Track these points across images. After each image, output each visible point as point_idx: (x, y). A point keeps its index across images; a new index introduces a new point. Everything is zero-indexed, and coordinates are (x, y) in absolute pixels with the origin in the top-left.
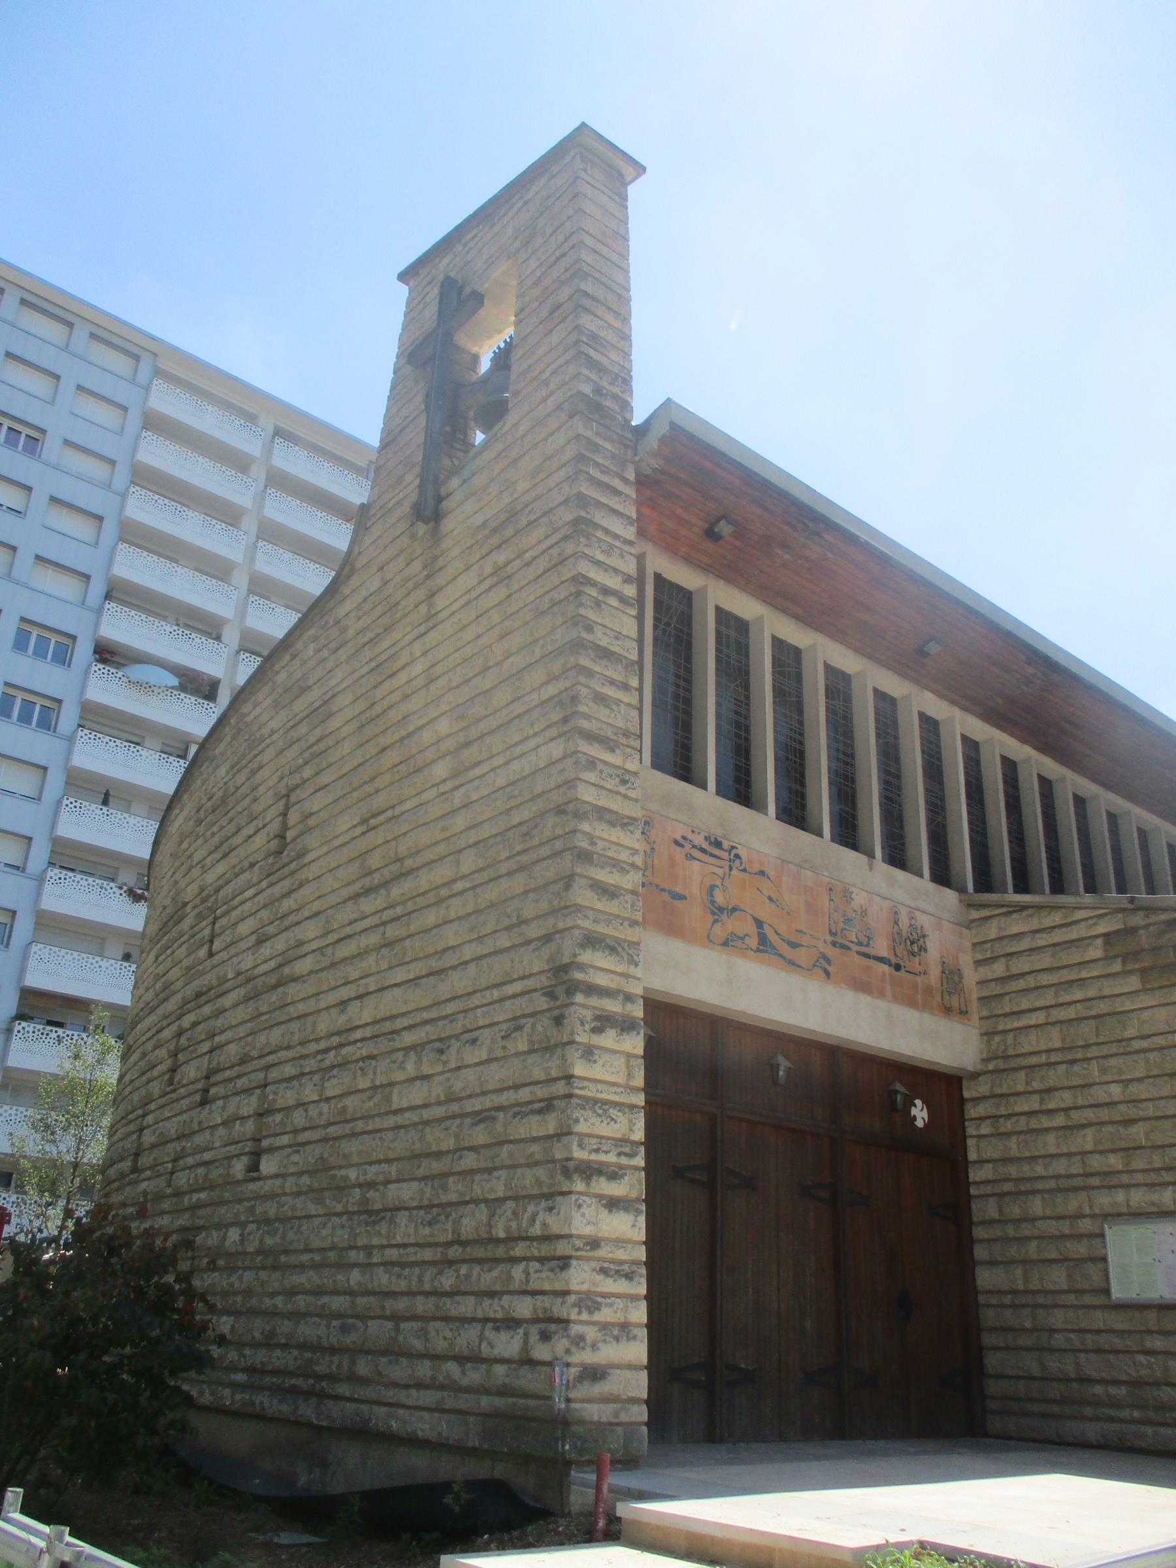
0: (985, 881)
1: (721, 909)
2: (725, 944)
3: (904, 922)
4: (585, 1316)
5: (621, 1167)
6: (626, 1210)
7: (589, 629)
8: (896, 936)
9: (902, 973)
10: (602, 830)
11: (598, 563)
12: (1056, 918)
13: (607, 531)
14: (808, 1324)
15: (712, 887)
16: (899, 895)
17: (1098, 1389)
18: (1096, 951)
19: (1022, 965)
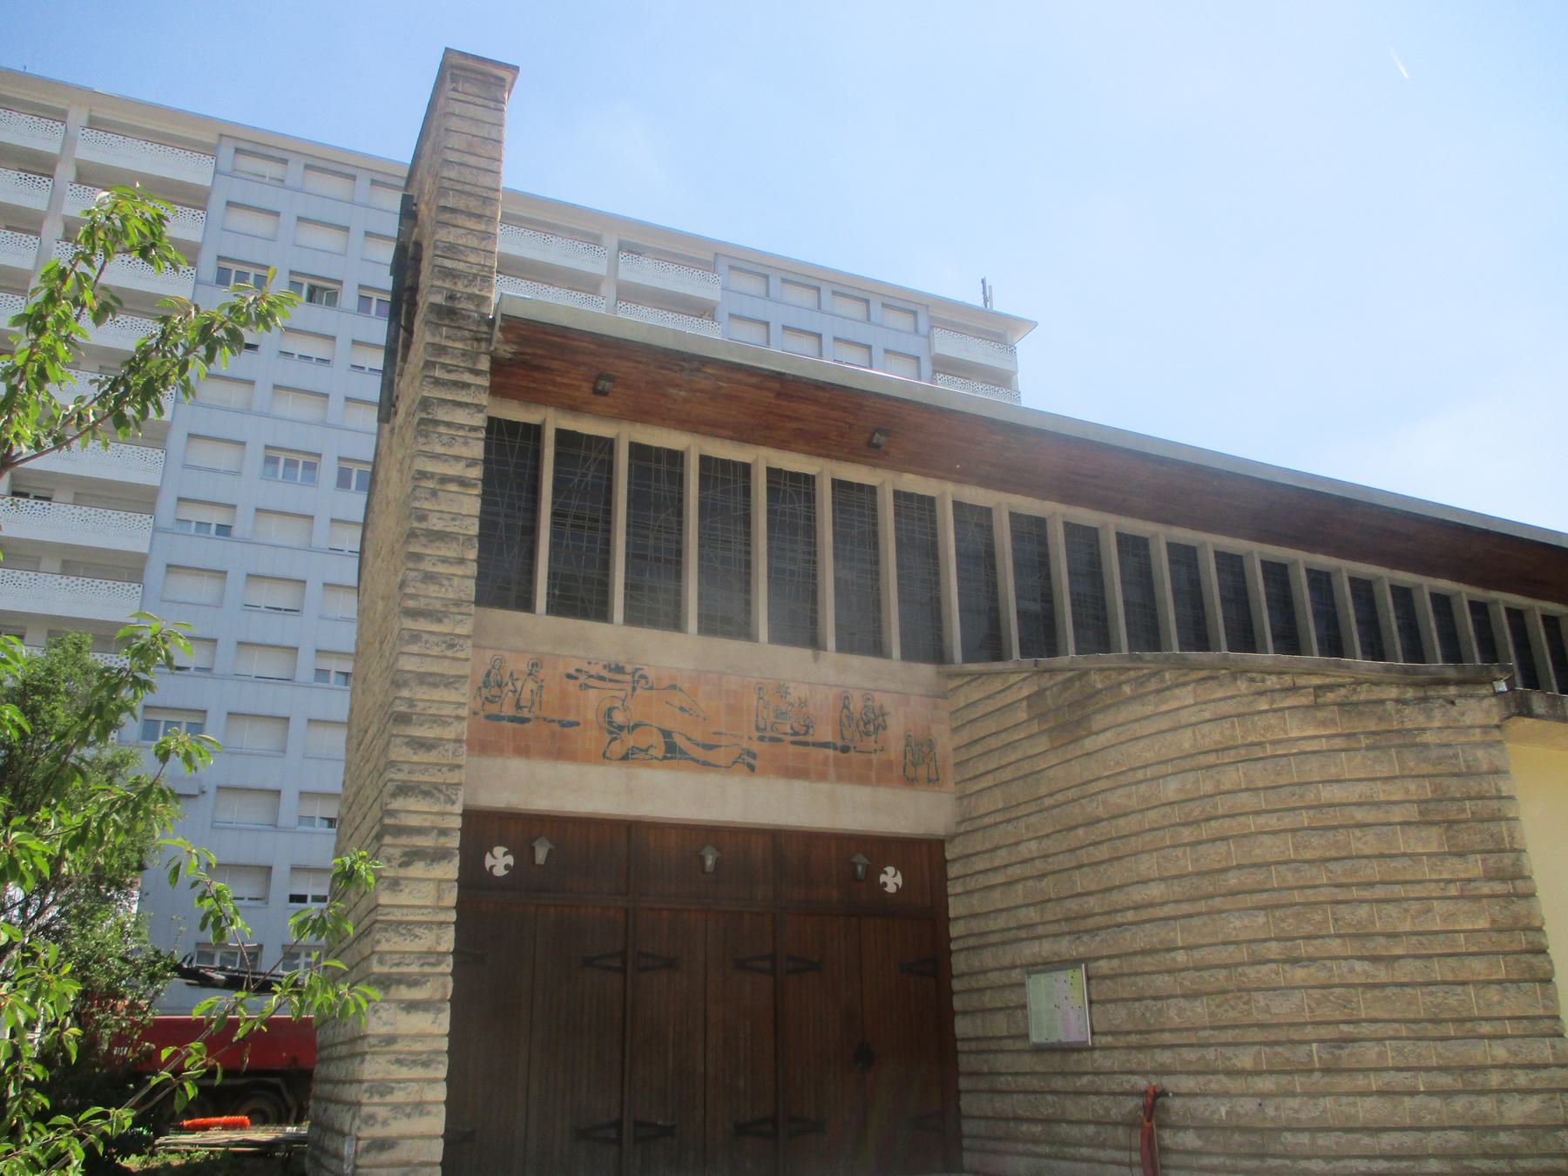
1: (621, 728)
2: (625, 758)
3: (857, 705)
4: (376, 1099)
5: (425, 975)
6: (426, 1010)
7: (422, 518)
8: (844, 720)
9: (852, 753)
10: (421, 693)
11: (435, 457)
12: (997, 684)
13: (449, 425)
14: (741, 1083)
15: (610, 710)
18: (1022, 715)
19: (980, 730)
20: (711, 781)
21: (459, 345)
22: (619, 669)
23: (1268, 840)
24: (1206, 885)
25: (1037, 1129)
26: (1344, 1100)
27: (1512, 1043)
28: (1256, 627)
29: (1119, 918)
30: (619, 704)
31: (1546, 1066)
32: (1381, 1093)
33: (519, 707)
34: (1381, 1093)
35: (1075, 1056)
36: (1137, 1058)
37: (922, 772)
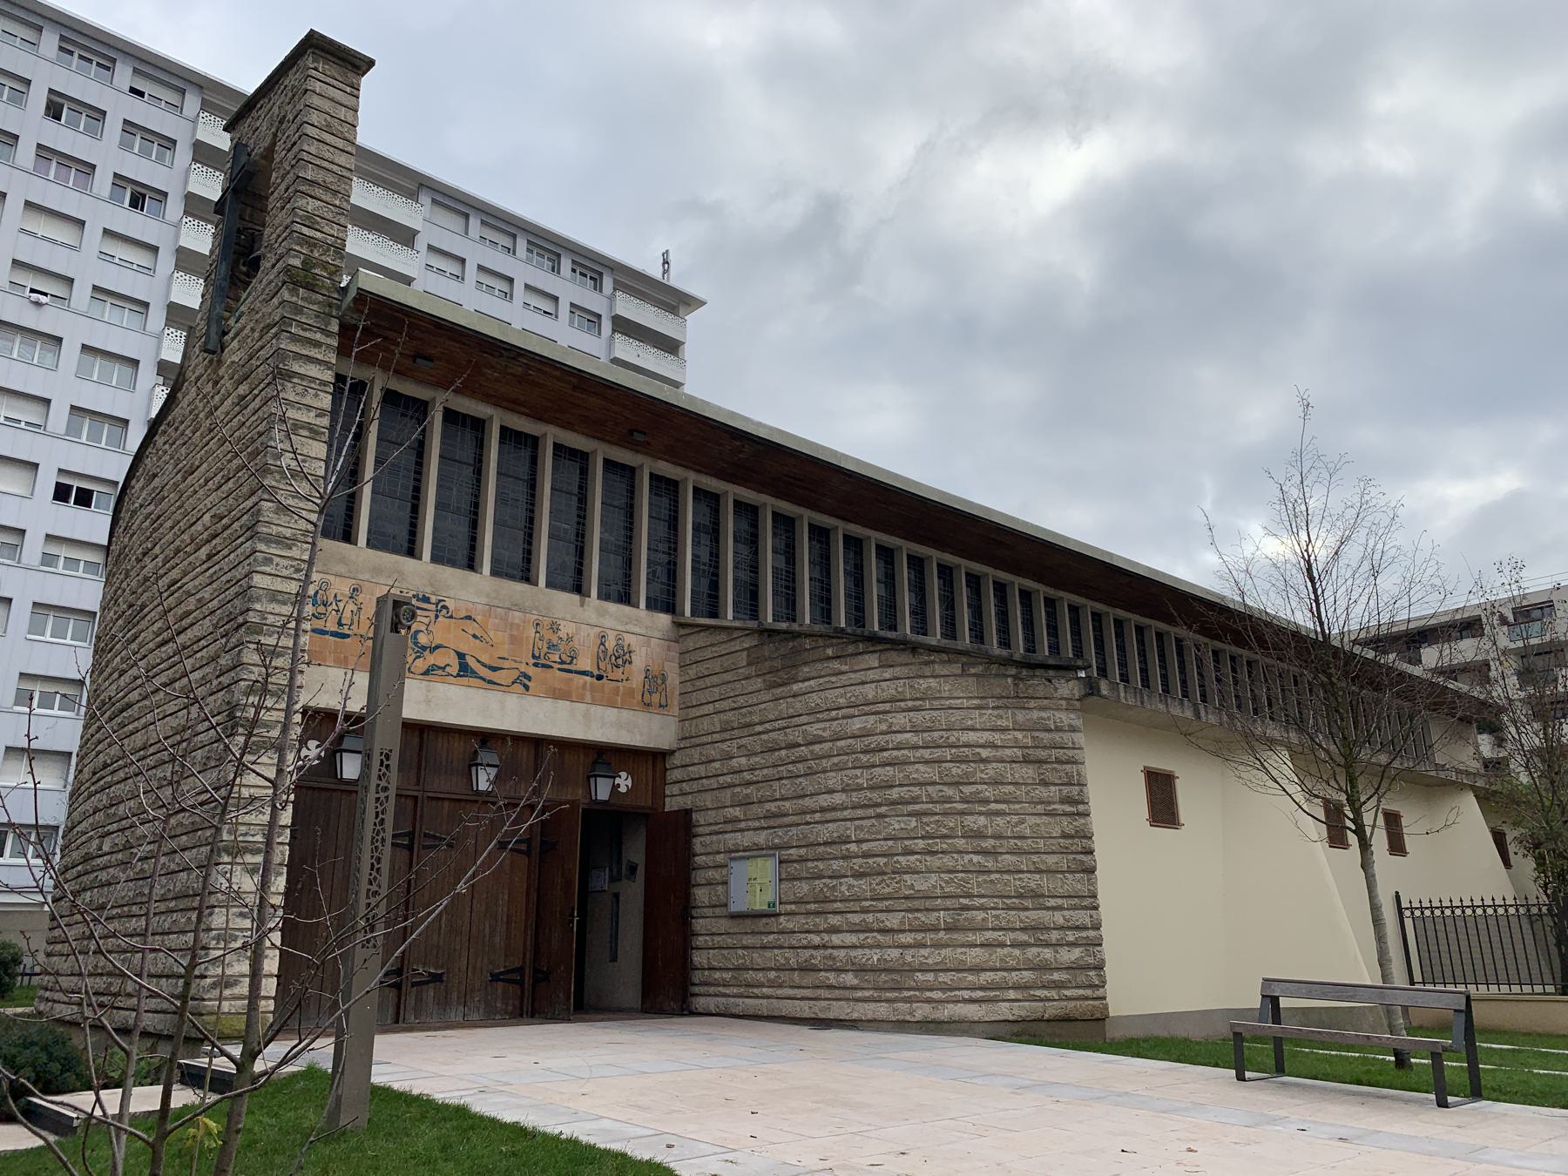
0: (710, 603)
1: (424, 648)
2: (426, 673)
3: (611, 644)
16: (608, 622)
17: (717, 975)
20: (493, 698)
21: (315, 307)
22: (426, 600)
23: (921, 767)
24: (875, 796)
25: (727, 976)
26: (960, 950)
27: (1066, 913)
28: (898, 603)
29: (808, 818)
30: (423, 628)
31: (1086, 928)
32: (982, 945)
33: (340, 624)
34: (982, 945)
35: (764, 920)
36: (811, 922)
37: (656, 698)
